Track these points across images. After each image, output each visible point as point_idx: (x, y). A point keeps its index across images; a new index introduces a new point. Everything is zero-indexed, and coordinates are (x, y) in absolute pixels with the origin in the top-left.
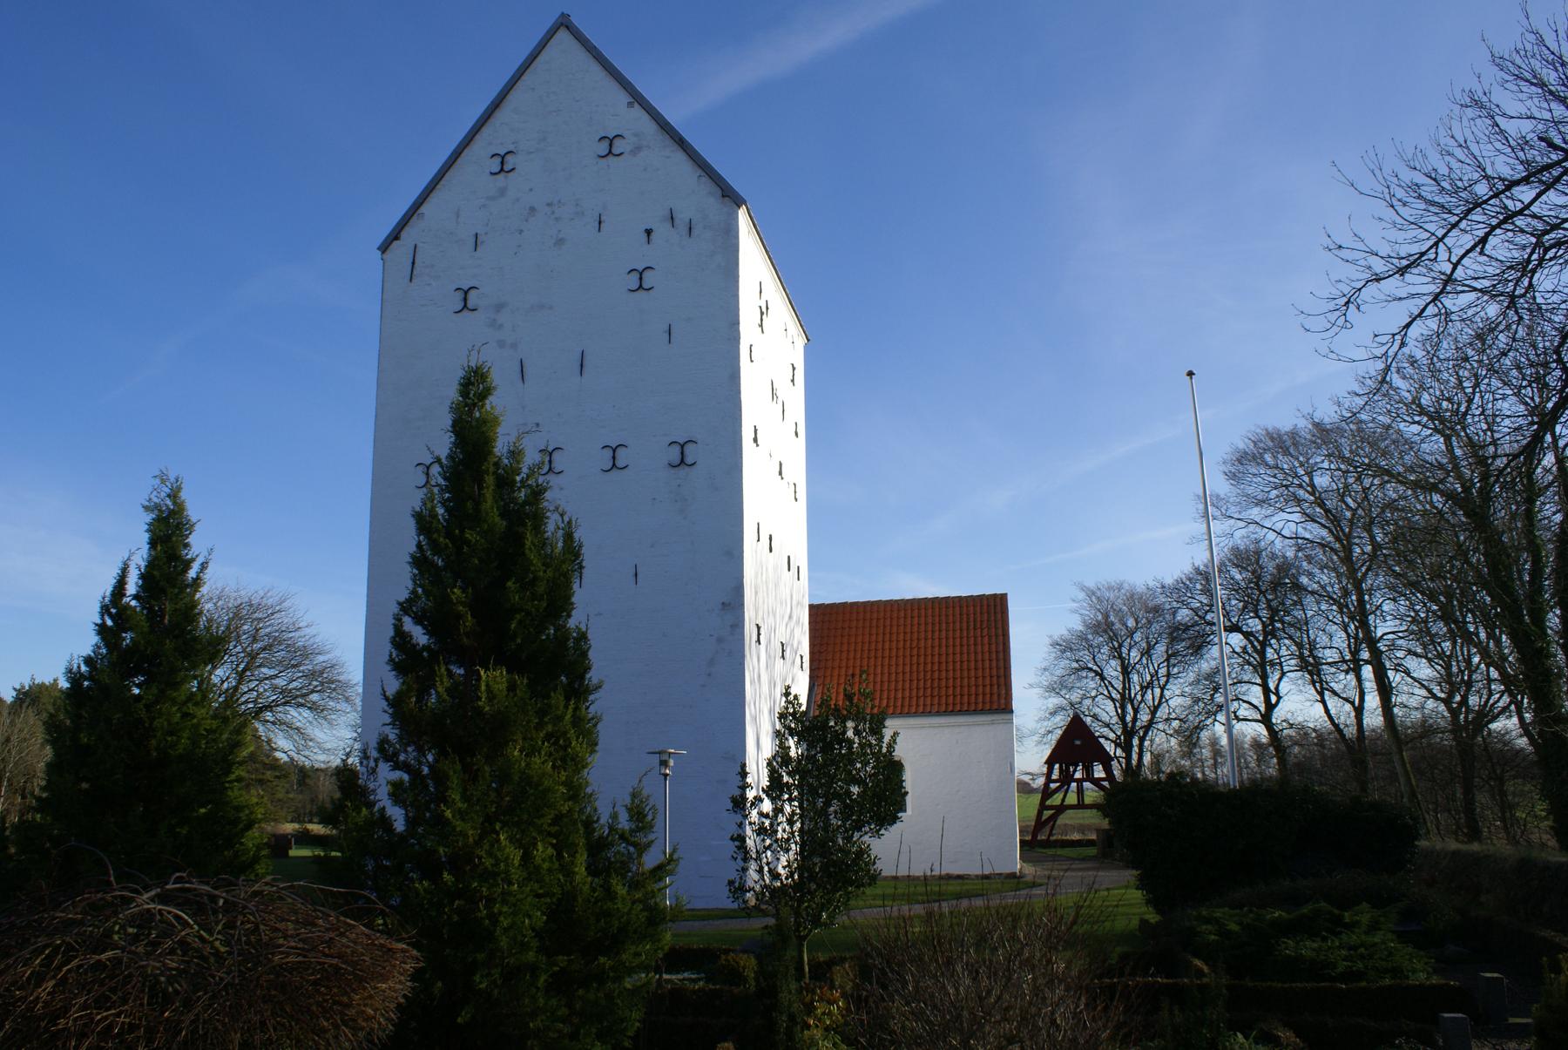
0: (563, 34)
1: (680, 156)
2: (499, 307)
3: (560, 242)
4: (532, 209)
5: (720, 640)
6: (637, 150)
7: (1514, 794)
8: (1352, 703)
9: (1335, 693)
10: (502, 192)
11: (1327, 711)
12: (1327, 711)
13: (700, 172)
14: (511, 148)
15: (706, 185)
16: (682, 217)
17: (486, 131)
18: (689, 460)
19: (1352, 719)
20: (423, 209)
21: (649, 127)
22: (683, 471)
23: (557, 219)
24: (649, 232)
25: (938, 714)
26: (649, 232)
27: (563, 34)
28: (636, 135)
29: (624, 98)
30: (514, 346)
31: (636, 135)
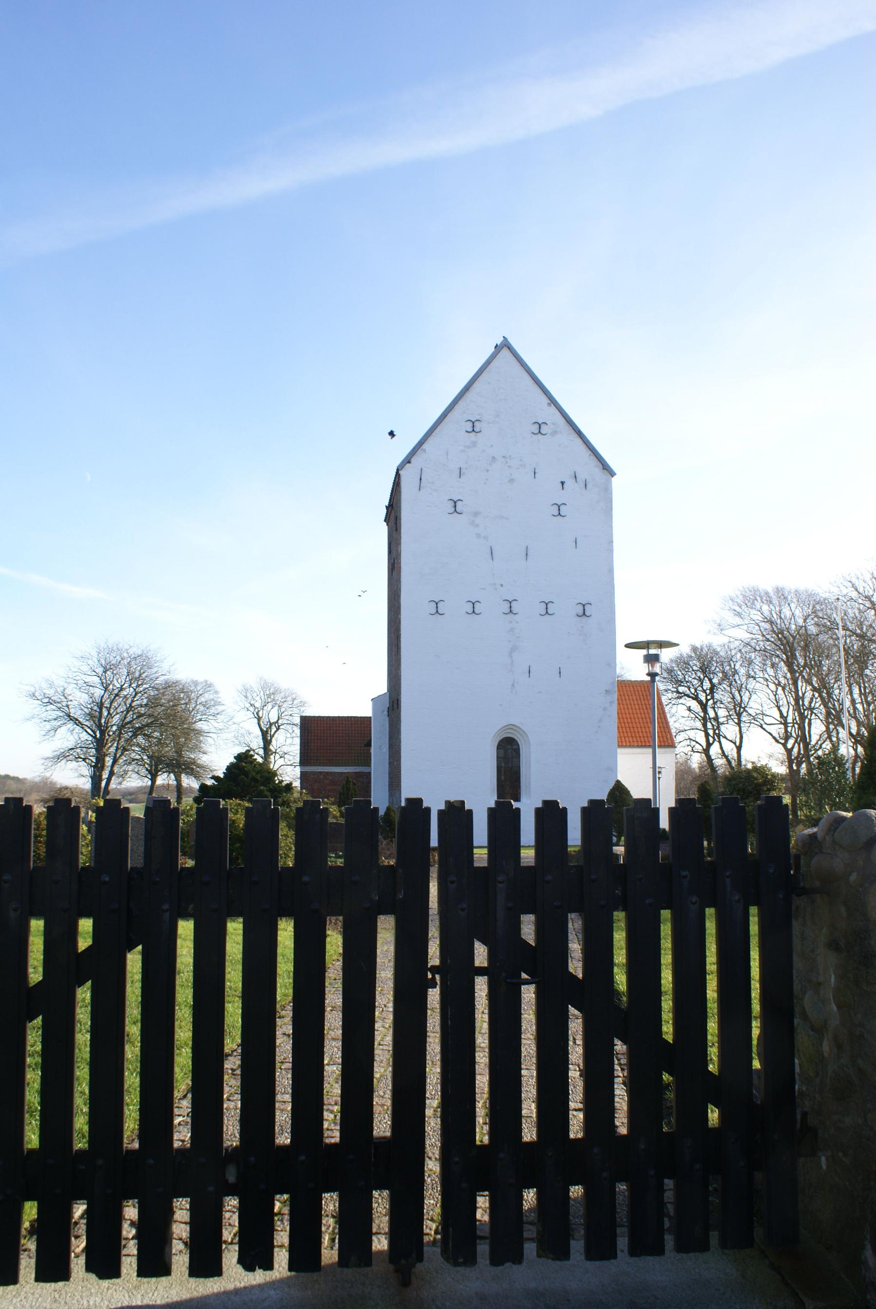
0: (505, 352)
1: (579, 441)
2: (476, 514)
3: (511, 481)
4: (494, 458)
5: (605, 709)
6: (554, 433)
7: (290, 849)
8: (735, 743)
9: (725, 737)
10: (474, 444)
11: (721, 748)
12: (721, 748)
13: (590, 452)
14: (478, 418)
15: (594, 461)
16: (581, 477)
17: (461, 403)
18: (587, 613)
19: (735, 755)
20: (424, 446)
21: (562, 421)
22: (584, 619)
23: (509, 467)
24: (563, 483)
25: (630, 746)
26: (563, 483)
27: (505, 352)
28: (554, 424)
29: (546, 400)
30: (486, 538)
31: (554, 424)
